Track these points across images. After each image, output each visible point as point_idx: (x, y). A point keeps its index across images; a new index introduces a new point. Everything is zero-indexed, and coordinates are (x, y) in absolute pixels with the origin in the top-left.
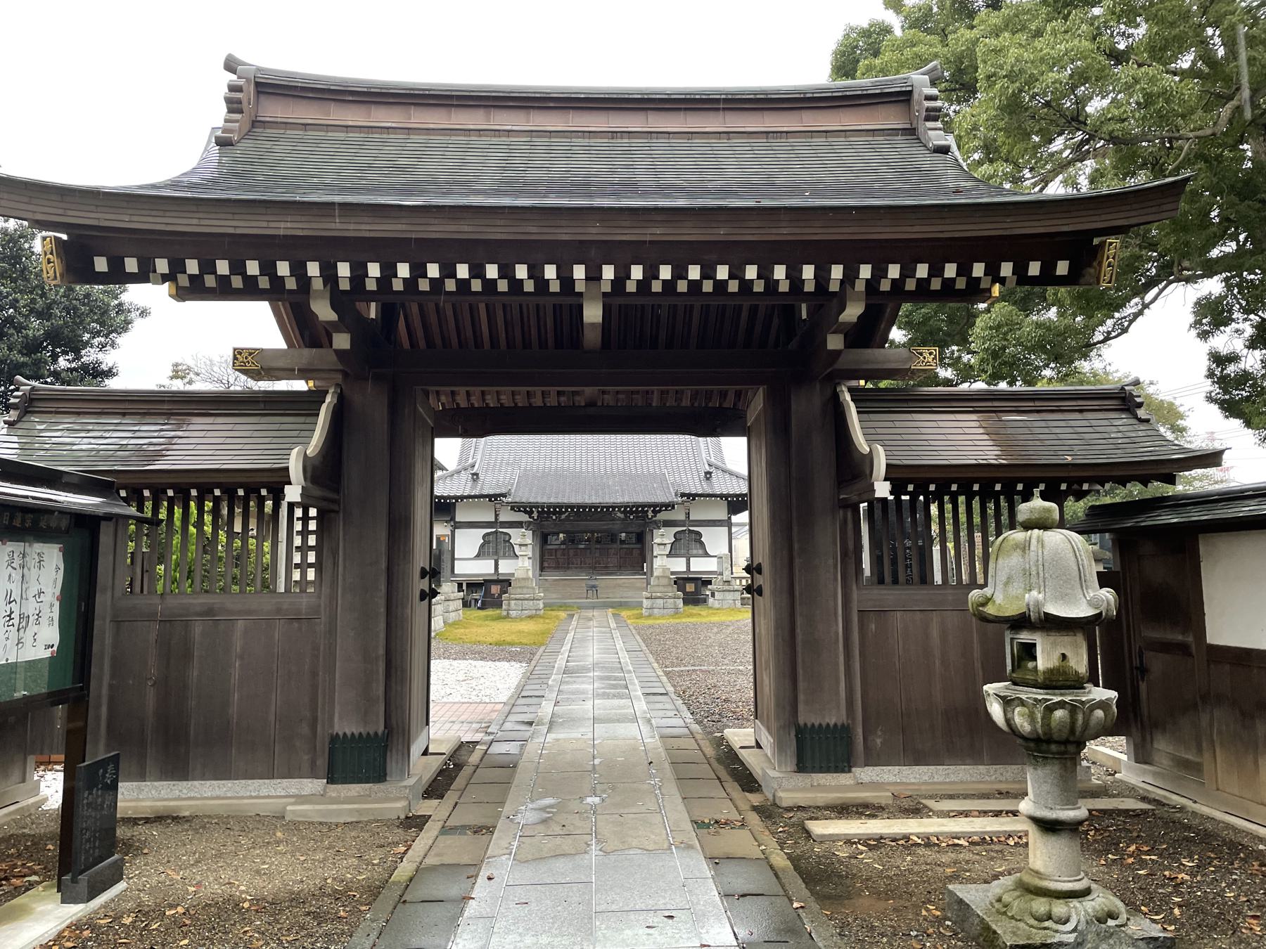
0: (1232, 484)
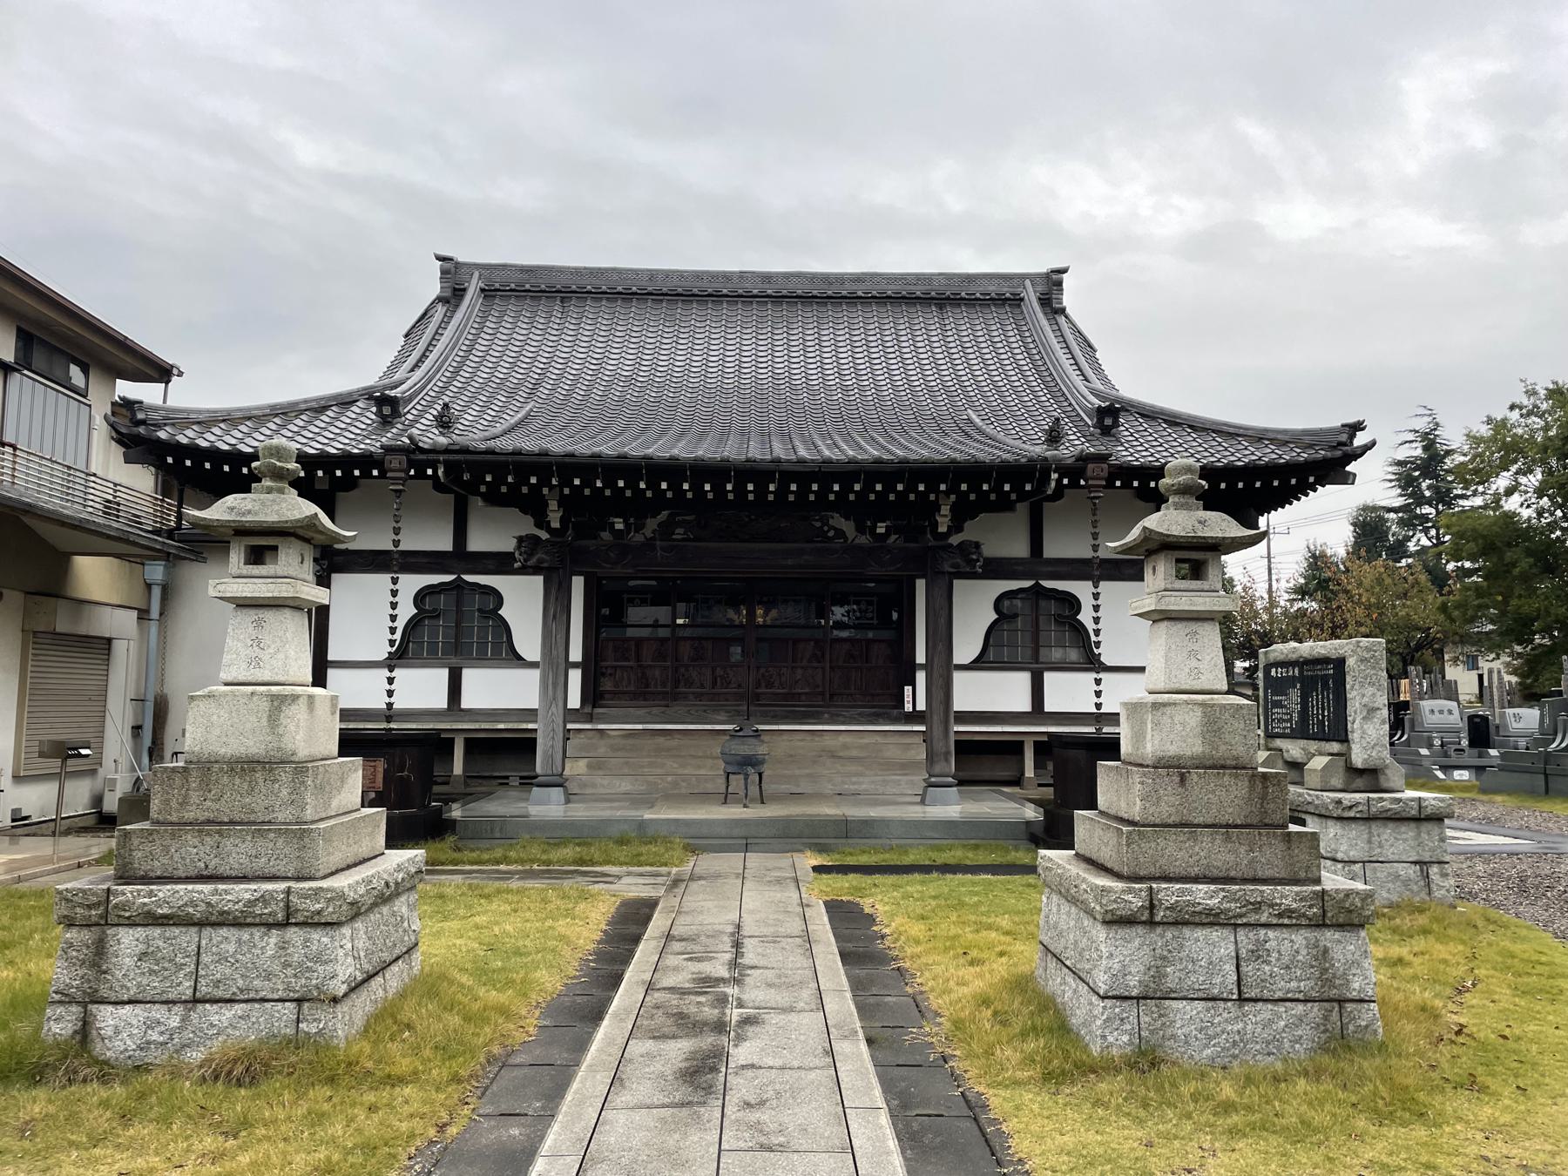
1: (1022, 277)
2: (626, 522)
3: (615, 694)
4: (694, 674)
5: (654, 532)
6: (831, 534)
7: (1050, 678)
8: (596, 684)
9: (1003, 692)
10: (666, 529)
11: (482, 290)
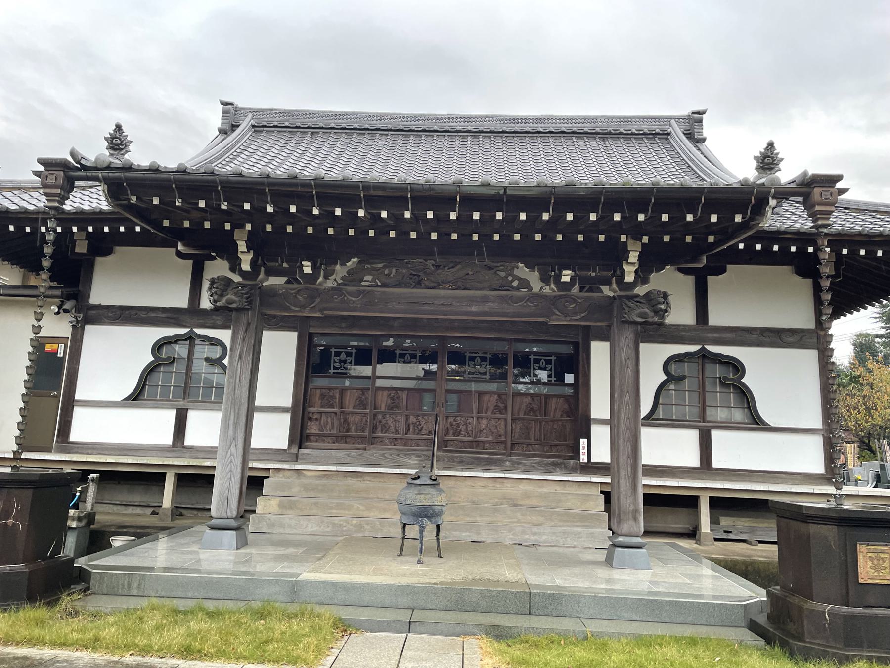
0: (617, 587)
1: (668, 119)
2: (314, 267)
3: (320, 437)
4: (390, 422)
5: (342, 278)
6: (515, 283)
7: (716, 436)
8: (303, 427)
9: (669, 448)
10: (353, 277)
11: (253, 126)
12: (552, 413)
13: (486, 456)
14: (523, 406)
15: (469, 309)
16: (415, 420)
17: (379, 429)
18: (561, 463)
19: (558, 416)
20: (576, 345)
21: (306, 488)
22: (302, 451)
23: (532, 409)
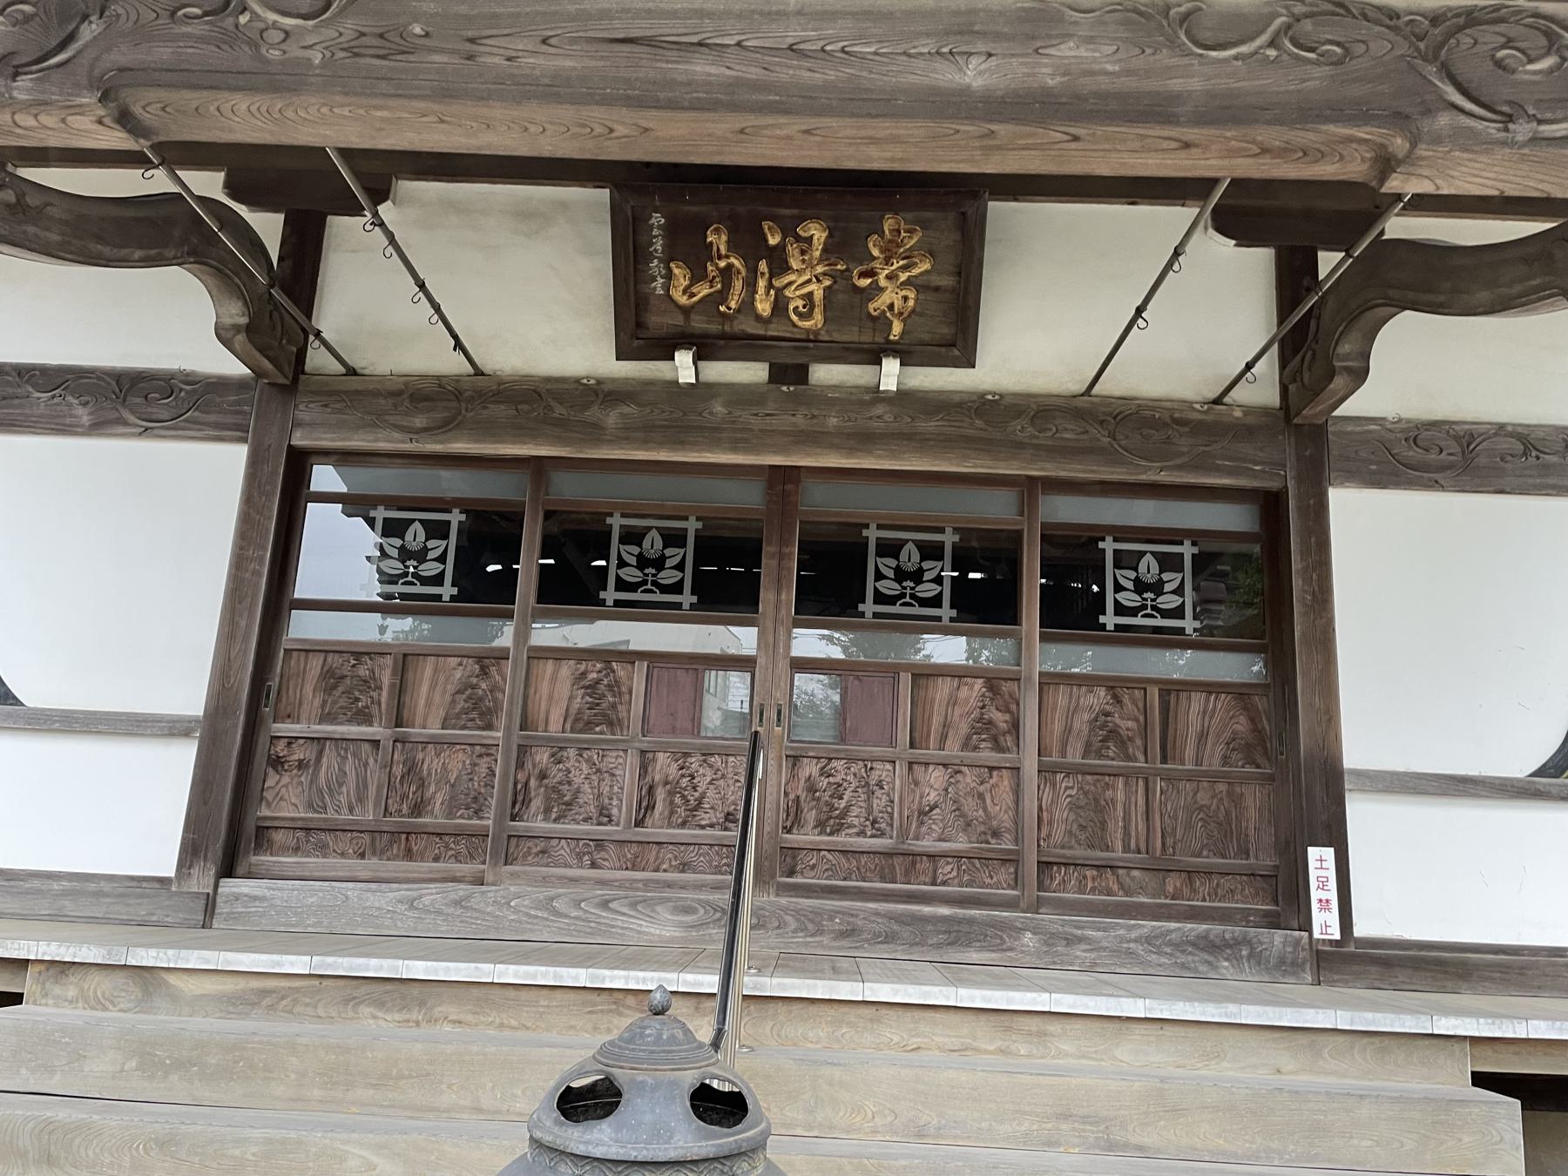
3: (312, 835)
12: (1189, 752)
13: (945, 911)
14: (1081, 722)
15: (948, 76)
16: (673, 771)
17: (537, 803)
18: (1236, 943)
19: (1213, 761)
20: (1271, 506)
21: (150, 1057)
22: (229, 886)
23: (1113, 734)
